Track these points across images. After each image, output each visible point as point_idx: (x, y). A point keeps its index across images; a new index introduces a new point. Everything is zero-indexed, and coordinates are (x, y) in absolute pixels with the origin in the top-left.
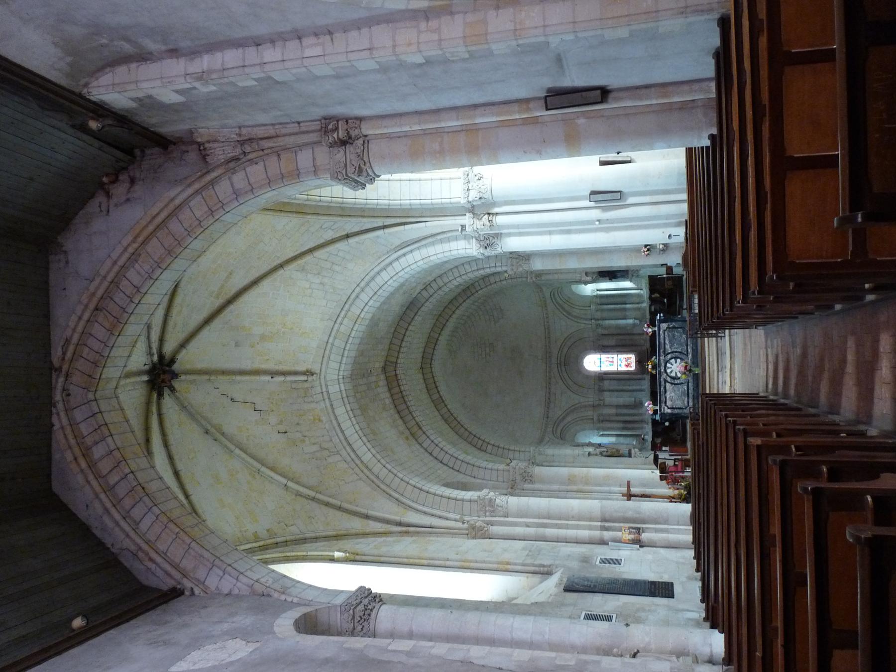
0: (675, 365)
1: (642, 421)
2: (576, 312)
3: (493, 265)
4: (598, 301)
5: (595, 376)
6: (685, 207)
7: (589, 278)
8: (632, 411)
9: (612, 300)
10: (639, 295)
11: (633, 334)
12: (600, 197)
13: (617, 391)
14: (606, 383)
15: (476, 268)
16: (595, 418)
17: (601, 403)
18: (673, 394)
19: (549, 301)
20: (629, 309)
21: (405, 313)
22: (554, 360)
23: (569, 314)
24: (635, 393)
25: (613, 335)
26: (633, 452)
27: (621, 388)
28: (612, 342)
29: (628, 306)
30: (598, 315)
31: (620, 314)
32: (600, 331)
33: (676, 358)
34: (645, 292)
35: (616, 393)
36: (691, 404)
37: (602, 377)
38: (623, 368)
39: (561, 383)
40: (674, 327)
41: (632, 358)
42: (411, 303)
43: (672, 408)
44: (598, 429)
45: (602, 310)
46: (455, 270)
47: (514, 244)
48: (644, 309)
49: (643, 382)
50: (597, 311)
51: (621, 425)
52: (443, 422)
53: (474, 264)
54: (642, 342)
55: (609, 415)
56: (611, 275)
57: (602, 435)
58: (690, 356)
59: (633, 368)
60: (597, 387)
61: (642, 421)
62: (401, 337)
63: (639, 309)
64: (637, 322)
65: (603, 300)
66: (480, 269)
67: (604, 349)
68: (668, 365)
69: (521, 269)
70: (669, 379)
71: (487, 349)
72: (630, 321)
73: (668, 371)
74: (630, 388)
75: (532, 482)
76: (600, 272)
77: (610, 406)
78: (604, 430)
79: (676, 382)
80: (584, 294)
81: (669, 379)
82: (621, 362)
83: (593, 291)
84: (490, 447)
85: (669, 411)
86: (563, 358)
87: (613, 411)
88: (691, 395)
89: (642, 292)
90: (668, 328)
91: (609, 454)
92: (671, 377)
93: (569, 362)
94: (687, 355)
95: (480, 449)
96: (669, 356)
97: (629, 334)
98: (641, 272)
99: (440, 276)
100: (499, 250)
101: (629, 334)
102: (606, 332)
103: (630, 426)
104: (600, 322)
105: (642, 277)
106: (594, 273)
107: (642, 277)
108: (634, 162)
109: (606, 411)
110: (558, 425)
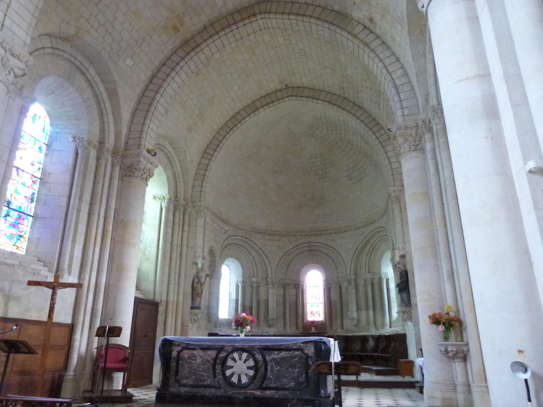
0: (245, 366)
2: (364, 259)
3: (405, 104)
4: (376, 281)
5: (300, 281)
7: (397, 259)
9: (377, 293)
10: (383, 325)
13: (284, 302)
14: (293, 291)
15: (398, 83)
18: (199, 360)
19: (372, 227)
20: (368, 314)
22: (313, 239)
23: (361, 252)
24: (282, 319)
25: (341, 297)
27: (287, 304)
28: (335, 297)
29: (371, 312)
30: (361, 282)
32: (345, 284)
33: (256, 368)
34: (387, 331)
35: (281, 300)
36: (183, 390)
38: (309, 309)
39: (291, 246)
40: (308, 367)
43: (178, 358)
44: (243, 282)
45: (365, 286)
48: (368, 330)
49: (294, 328)
50: (365, 280)
52: (232, 115)
54: (334, 328)
55: (258, 293)
57: (237, 286)
58: (258, 393)
60: (289, 282)
62: (302, 12)
63: (368, 324)
64: (355, 323)
65: (376, 285)
68: (245, 355)
70: (223, 355)
71: (320, 172)
72: (355, 315)
73: (236, 355)
74: (287, 316)
75: (122, 177)
76: (406, 272)
78: (244, 288)
79: (218, 367)
81: (223, 355)
82: (315, 309)
85: (174, 354)
86: (316, 248)
87: (262, 297)
88: (195, 390)
89: (388, 327)
90: (307, 357)
91: (195, 284)
92: (225, 359)
93: (313, 254)
95: (205, 152)
96: (259, 357)
98: (409, 324)
99: (384, 43)
102: (344, 290)
104: (353, 283)
105: (403, 326)
106: (405, 265)
107: (403, 326)
109: (262, 290)
110: (246, 243)
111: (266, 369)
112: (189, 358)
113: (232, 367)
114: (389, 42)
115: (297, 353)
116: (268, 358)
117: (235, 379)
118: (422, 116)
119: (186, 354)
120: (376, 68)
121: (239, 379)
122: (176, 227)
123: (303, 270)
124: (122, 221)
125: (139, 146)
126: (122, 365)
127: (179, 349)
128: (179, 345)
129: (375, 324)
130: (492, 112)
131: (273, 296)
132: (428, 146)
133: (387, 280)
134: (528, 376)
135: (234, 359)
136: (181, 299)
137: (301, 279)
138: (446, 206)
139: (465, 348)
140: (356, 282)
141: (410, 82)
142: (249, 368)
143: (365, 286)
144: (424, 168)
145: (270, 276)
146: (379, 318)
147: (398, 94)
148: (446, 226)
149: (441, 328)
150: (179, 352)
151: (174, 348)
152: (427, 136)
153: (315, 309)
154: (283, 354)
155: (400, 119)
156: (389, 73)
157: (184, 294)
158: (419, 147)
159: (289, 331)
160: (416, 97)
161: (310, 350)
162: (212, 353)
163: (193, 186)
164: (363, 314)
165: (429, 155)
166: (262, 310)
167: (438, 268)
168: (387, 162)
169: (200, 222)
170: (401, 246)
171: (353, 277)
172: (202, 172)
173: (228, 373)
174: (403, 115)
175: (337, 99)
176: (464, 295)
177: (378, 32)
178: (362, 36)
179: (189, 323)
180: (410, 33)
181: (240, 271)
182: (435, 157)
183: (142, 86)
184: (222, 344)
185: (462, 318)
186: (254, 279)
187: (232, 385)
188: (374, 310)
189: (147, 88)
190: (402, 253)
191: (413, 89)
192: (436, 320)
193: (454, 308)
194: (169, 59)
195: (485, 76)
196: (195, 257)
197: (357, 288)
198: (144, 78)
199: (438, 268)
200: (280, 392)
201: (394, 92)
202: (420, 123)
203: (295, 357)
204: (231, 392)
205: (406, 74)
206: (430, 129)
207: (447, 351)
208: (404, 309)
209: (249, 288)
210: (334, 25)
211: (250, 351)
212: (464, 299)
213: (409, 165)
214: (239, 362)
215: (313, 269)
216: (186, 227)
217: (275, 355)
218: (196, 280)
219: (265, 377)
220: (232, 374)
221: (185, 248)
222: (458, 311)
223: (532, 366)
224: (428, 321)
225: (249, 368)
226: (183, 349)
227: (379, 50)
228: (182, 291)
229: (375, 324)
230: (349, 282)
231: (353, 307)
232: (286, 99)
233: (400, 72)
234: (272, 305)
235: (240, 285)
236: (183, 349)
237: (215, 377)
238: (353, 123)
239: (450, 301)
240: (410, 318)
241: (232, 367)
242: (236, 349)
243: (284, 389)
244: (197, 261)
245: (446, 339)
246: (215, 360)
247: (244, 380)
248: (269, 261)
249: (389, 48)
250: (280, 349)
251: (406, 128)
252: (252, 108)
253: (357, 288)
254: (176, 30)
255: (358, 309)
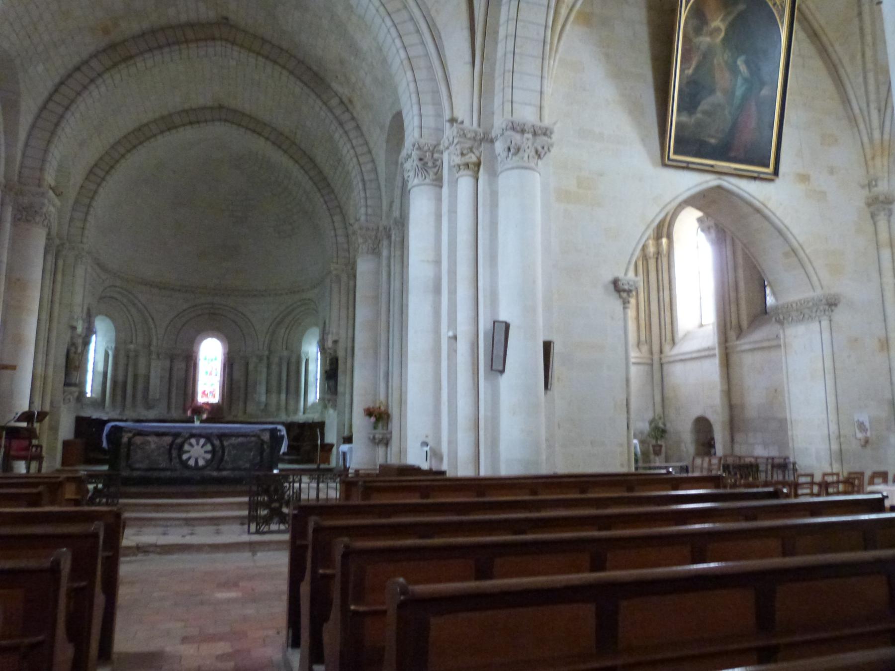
0: (202, 451)
1: (124, 406)
3: (369, 202)
4: (293, 360)
6: (464, 471)
7: (329, 344)
8: (139, 395)
9: (293, 374)
10: (296, 410)
11: (245, 403)
12: (500, 337)
15: (366, 178)
16: (132, 346)
17: (154, 356)
21: (309, 68)
23: (279, 323)
26: (73, 389)
27: (175, 382)
28: (238, 375)
29: (283, 396)
30: (275, 360)
31: (274, 383)
32: (253, 361)
33: (213, 452)
34: (300, 417)
35: (167, 375)
36: (136, 474)
37: (190, 362)
41: (215, 399)
42: (322, 80)
44: (117, 350)
45: (280, 365)
46: (365, 149)
47: (420, 206)
51: (120, 378)
53: (373, 176)
55: (135, 366)
56: (331, 374)
58: (215, 474)
59: (201, 399)
61: (124, 406)
63: (278, 409)
64: (262, 407)
65: (293, 367)
66: (364, 185)
67: (229, 365)
69: (360, 240)
70: (179, 440)
72: (263, 398)
73: (193, 441)
74: (174, 395)
75: (16, 221)
77: (149, 366)
78: (116, 357)
79: (174, 453)
80: (303, 344)
81: (179, 440)
82: (209, 385)
83: (307, 353)
84: (93, 187)
85: (125, 440)
87: (142, 371)
89: (301, 413)
90: (263, 442)
91: (72, 355)
92: (181, 446)
94: (219, 469)
96: (217, 443)
97: (246, 394)
99: (358, 127)
100: (414, 181)
101: (246, 394)
102: (251, 367)
103: (119, 392)
108: (546, 393)
109: (142, 362)
111: (223, 453)
112: (142, 444)
113: (188, 452)
114: (364, 129)
115: (253, 439)
116: (226, 443)
117: (192, 463)
118: (384, 222)
119: (138, 440)
120: (346, 151)
121: (196, 462)
122: (48, 276)
123: (198, 338)
124: (19, 280)
125: (40, 183)
126: (23, 453)
127: (130, 435)
128: (130, 432)
129: (286, 409)
130: (437, 290)
131: (157, 371)
132: (385, 253)
133: (307, 361)
134: (427, 449)
135: (191, 445)
136: (50, 372)
137: (195, 349)
138: (391, 313)
139: (388, 436)
140: (268, 358)
141: (377, 179)
142: (206, 452)
143: (280, 365)
144: (378, 273)
145: (154, 342)
146: (292, 402)
147: (365, 190)
148: (388, 332)
149: (373, 419)
150: (130, 439)
151: (124, 434)
152: (385, 242)
153: (209, 385)
154: (240, 440)
155: (363, 218)
156: (360, 164)
157: (55, 366)
158: (375, 251)
159: (175, 414)
160: (380, 198)
161: (266, 437)
162: (168, 440)
163: (72, 219)
164: (274, 396)
165: (384, 262)
166: (140, 386)
167: (376, 367)
168: (332, 233)
169: (80, 271)
170: (334, 331)
171: (267, 353)
172: (86, 201)
173: (185, 457)
174: (366, 214)
175: (282, 141)
176: (394, 392)
177: (355, 115)
178: (338, 112)
179: (62, 404)
180: (387, 142)
181: (113, 334)
182: (389, 266)
183: (46, 94)
184: (179, 430)
185: (390, 412)
186: (132, 346)
187: (187, 467)
188: (287, 394)
189: (50, 99)
190: (335, 338)
191: (379, 188)
192: (369, 413)
193: (384, 402)
194: (86, 62)
195: (438, 262)
196: (72, 318)
197: (269, 367)
198: (50, 85)
199: (376, 367)
200: (236, 472)
201: (360, 185)
202: (381, 228)
203: (252, 442)
204: (187, 474)
205: (375, 170)
206: (389, 237)
207: (374, 438)
208: (328, 397)
209: (123, 356)
210: (309, 87)
211: (208, 438)
212: (395, 396)
213: (364, 267)
214: (196, 447)
215: (212, 337)
216: (59, 277)
217: (233, 441)
218: (73, 349)
219: (222, 460)
220: (189, 458)
221: (56, 306)
222: (387, 406)
223: (431, 444)
224: (362, 413)
225: (206, 452)
226: (135, 435)
227: (352, 134)
228: (51, 364)
229: (286, 409)
230: (260, 359)
231: (262, 389)
232: (217, 123)
233: (369, 166)
234: (155, 381)
235: (111, 353)
236: (135, 435)
237: (171, 460)
238: (296, 172)
239: (382, 397)
240: (335, 406)
241: (188, 452)
242: (192, 436)
243: (239, 469)
244: (74, 324)
245: (375, 428)
246: (171, 445)
247: (201, 463)
248: (154, 323)
249: (362, 135)
250: (238, 435)
251: (368, 229)
252: (168, 123)
253: (269, 367)
254: (106, 31)
255: (268, 391)
